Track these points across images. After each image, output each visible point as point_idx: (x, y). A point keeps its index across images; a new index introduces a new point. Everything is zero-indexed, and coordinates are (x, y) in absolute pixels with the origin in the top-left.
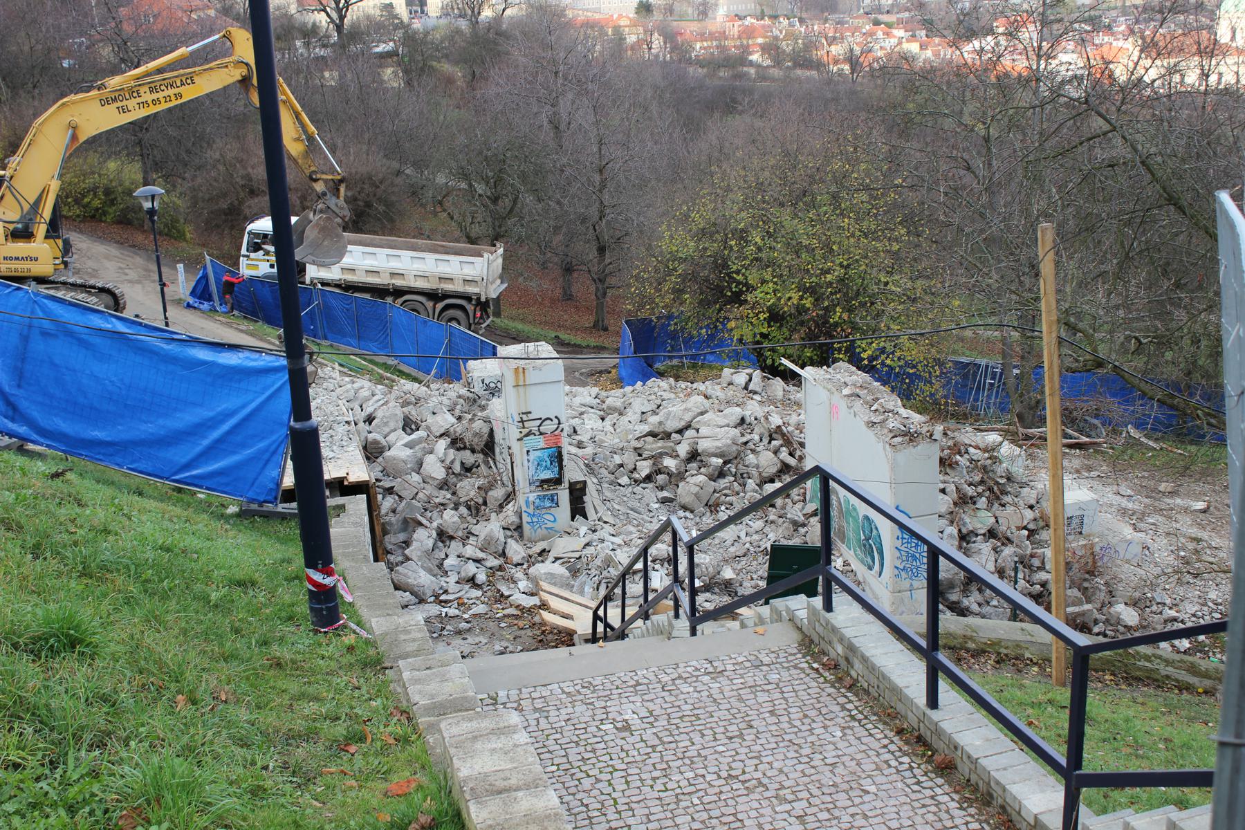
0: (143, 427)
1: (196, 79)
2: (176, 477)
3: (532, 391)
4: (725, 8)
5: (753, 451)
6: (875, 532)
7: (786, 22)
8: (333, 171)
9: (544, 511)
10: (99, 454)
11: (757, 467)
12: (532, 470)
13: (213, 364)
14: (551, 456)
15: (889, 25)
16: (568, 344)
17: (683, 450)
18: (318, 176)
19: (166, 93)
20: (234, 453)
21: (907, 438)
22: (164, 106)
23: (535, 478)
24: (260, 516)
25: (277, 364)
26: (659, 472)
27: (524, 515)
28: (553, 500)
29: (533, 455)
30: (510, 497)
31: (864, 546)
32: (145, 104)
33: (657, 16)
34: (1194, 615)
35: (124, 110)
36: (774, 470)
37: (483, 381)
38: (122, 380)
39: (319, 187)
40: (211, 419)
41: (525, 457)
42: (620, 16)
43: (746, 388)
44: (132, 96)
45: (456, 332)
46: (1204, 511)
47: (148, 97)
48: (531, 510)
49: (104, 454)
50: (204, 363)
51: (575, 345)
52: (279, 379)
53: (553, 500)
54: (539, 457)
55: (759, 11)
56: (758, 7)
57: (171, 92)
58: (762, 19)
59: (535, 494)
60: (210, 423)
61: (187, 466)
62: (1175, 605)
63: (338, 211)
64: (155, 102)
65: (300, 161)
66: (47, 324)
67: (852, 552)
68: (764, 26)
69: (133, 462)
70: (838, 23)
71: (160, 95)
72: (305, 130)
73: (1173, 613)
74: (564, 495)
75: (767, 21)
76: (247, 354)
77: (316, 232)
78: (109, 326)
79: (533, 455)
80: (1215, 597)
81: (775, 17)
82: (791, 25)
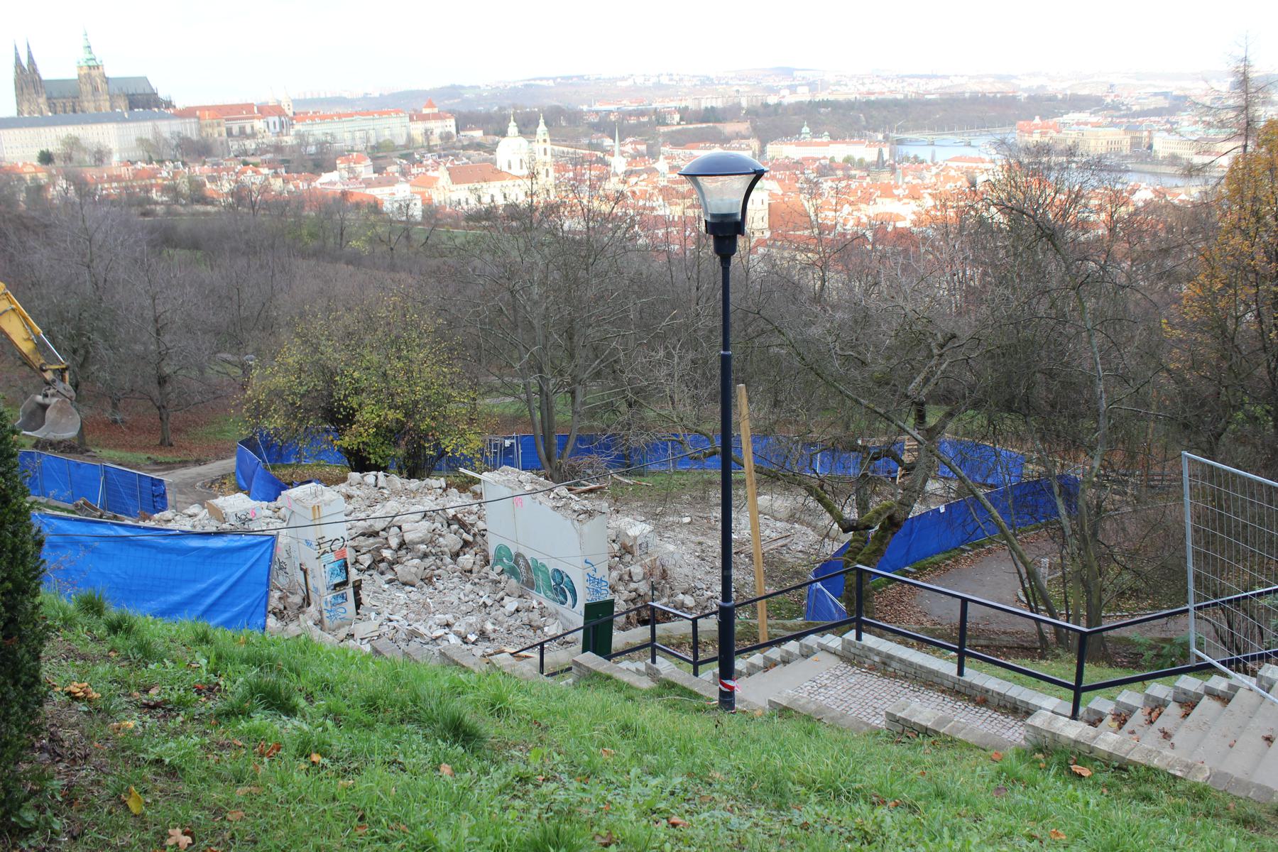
4: (118, 155)
5: (440, 535)
7: (171, 165)
11: (446, 546)
12: (328, 578)
14: (340, 566)
15: (256, 165)
16: (161, 463)
17: (394, 542)
20: (225, 612)
27: (325, 612)
29: (328, 567)
30: (307, 601)
31: (556, 589)
33: (59, 163)
40: (204, 590)
42: (25, 164)
45: (112, 471)
46: (689, 523)
48: (329, 608)
51: (168, 463)
52: (257, 552)
55: (147, 158)
56: (146, 154)
58: (151, 163)
63: (65, 393)
65: (31, 357)
67: (542, 595)
68: (153, 169)
70: (214, 165)
73: (709, 593)
74: (350, 591)
75: (155, 165)
76: (230, 537)
78: (112, 533)
79: (328, 567)
81: (161, 162)
82: (175, 167)
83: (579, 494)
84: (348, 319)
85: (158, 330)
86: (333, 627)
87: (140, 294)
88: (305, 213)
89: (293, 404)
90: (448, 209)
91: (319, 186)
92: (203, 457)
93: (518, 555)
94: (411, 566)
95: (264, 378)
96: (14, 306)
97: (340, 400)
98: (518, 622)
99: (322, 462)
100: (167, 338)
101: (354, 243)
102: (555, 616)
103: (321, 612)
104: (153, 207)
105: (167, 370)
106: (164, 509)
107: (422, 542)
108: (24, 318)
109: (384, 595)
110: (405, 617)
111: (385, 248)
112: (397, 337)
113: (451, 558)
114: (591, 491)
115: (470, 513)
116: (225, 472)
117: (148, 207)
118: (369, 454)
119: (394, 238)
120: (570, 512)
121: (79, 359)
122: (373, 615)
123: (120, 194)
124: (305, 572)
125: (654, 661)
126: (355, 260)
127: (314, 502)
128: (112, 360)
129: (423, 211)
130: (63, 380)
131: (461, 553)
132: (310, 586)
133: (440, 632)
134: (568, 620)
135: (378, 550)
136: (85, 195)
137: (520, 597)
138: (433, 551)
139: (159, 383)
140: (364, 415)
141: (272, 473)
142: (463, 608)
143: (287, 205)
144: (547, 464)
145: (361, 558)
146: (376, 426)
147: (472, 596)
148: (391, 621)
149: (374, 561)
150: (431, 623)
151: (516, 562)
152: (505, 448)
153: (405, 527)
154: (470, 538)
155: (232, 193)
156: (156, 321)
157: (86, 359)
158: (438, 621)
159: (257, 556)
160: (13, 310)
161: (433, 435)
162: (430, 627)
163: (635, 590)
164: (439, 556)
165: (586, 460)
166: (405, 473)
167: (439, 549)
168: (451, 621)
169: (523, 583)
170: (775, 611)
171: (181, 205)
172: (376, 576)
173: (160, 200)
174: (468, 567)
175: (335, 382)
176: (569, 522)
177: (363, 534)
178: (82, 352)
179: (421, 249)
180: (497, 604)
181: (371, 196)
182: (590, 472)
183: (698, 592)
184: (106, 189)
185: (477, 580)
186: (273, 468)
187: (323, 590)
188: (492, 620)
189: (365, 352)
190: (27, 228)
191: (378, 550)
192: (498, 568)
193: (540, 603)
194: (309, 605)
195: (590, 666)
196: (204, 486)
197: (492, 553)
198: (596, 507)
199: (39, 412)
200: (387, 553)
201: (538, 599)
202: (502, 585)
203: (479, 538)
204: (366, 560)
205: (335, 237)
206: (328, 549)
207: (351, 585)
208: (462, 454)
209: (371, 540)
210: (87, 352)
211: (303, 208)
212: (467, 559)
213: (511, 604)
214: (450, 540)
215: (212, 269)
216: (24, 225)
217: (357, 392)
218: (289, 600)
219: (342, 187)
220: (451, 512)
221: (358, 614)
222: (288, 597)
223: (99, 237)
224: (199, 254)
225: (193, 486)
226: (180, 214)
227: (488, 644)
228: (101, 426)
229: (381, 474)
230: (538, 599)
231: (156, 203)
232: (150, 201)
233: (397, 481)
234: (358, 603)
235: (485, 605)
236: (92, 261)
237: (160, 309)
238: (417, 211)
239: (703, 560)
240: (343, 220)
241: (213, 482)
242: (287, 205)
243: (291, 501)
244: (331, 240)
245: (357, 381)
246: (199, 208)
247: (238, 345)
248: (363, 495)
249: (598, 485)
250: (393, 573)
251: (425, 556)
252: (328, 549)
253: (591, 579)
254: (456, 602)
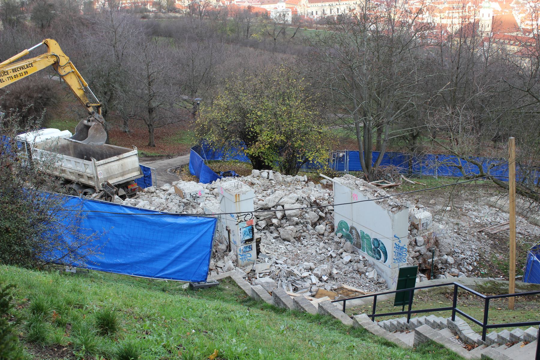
0: (140, 255)
1: (33, 64)
2: (158, 275)
3: (241, 203)
5: (306, 212)
6: (381, 245)
8: (96, 102)
9: (247, 253)
10: (119, 269)
11: (309, 219)
12: (242, 236)
13: (176, 224)
14: (249, 230)
17: (279, 215)
18: (90, 105)
19: (20, 72)
20: (185, 262)
21: (398, 208)
22: (20, 78)
23: (243, 240)
24: (201, 288)
25: (205, 221)
27: (239, 256)
28: (250, 248)
29: (243, 230)
32: (11, 78)
34: (470, 256)
36: (316, 220)
37: (190, 194)
38: (129, 235)
39: (91, 110)
40: (173, 248)
41: (239, 231)
43: (268, 178)
44: (4, 75)
46: (450, 211)
47: (13, 74)
48: (241, 254)
49: (121, 269)
50: (170, 224)
51: (152, 156)
53: (250, 248)
54: (245, 231)
57: (22, 71)
59: (243, 246)
60: (173, 250)
61: (163, 270)
62: (462, 252)
63: (100, 120)
64: (16, 76)
65: (81, 99)
66: (89, 213)
67: (366, 253)
69: (136, 271)
71: (18, 73)
73: (463, 256)
74: (254, 244)
76: (191, 218)
77: (93, 130)
78: (122, 212)
80: (474, 247)
83: (384, 188)
84: (256, 81)
85: (149, 82)
86: (243, 264)
87: (141, 63)
88: (228, 18)
89: (223, 128)
90: (306, 17)
91: (236, 3)
92: (171, 154)
93: (352, 228)
94: (289, 230)
95: (207, 112)
96: (73, 70)
97: (249, 127)
98: (351, 269)
99: (236, 161)
100: (154, 88)
101: (254, 35)
102: (373, 266)
103: (237, 256)
104: (148, 13)
105: (154, 105)
106: (150, 185)
107: (295, 216)
108: (79, 77)
109: (272, 246)
110: (285, 262)
111: (271, 38)
112: (283, 93)
113: (312, 226)
114: (390, 187)
115: (324, 199)
116: (183, 163)
117: (145, 13)
118: (264, 159)
119: (276, 33)
120: (387, 206)
121: (108, 98)
122: (267, 259)
123: (131, 6)
124: (229, 232)
125: (453, 319)
126: (255, 45)
127: (237, 191)
128: (125, 99)
129: (292, 18)
130: (98, 112)
131: (318, 224)
132: (231, 240)
133: (306, 274)
134: (380, 269)
135: (270, 219)
136: (113, 7)
137: (352, 253)
138: (302, 221)
139: (149, 112)
140: (263, 137)
141: (208, 165)
142: (319, 257)
143: (219, 13)
144: (366, 170)
145: (259, 223)
146: (269, 144)
147: (324, 250)
148: (277, 264)
149: (267, 225)
150: (301, 268)
151: (351, 232)
152: (340, 158)
153: (286, 207)
154: (323, 215)
155: (189, 7)
156: (149, 77)
157: (111, 97)
158: (305, 267)
159: (206, 229)
160: (73, 72)
161: (302, 151)
162: (301, 270)
163: (419, 251)
164: (305, 224)
165: (388, 168)
166: (284, 172)
167: (305, 220)
168: (313, 266)
169: (354, 244)
170: (503, 270)
171: (163, 13)
172: (268, 234)
173: (151, 10)
174: (322, 232)
175: (247, 118)
176: (386, 211)
177: (261, 209)
178: (109, 93)
179: (291, 39)
180: (338, 256)
181: (264, 9)
182: (389, 175)
183: (456, 255)
184: (124, 3)
185: (327, 241)
186: (209, 162)
187: (239, 243)
188: (335, 266)
189: (265, 100)
190: (83, 24)
191: (270, 219)
192: (339, 235)
193: (364, 258)
194: (230, 251)
195: (427, 335)
196: (171, 171)
197: (336, 225)
198: (403, 204)
199: (85, 130)
200: (275, 221)
201: (364, 254)
202: (342, 245)
203: (328, 215)
204: (263, 224)
205: (244, 32)
206: (243, 220)
207: (255, 241)
208: (317, 162)
209: (266, 213)
210: (112, 94)
211: (227, 15)
212: (321, 228)
213: (347, 257)
214: (312, 215)
215: (179, 48)
216: (83, 23)
217: (259, 123)
218: (219, 247)
219: (248, 4)
220: (313, 199)
221: (258, 258)
222: (218, 245)
223: (120, 30)
224: (171, 40)
225: (166, 171)
226: (162, 18)
227: (334, 282)
228: (118, 134)
229: (271, 171)
230: (364, 254)
231: (150, 12)
232: (147, 10)
233: (280, 176)
234: (258, 252)
235: (331, 256)
236: (116, 43)
237: (151, 71)
238: (289, 18)
239: (459, 234)
240: (249, 22)
241: (176, 169)
242: (219, 13)
243: (223, 190)
244: (242, 33)
245: (260, 116)
246: (172, 14)
247: (193, 92)
248: (260, 183)
249: (394, 184)
250: (277, 233)
251: (297, 224)
252: (243, 220)
253: (397, 247)
254: (314, 253)
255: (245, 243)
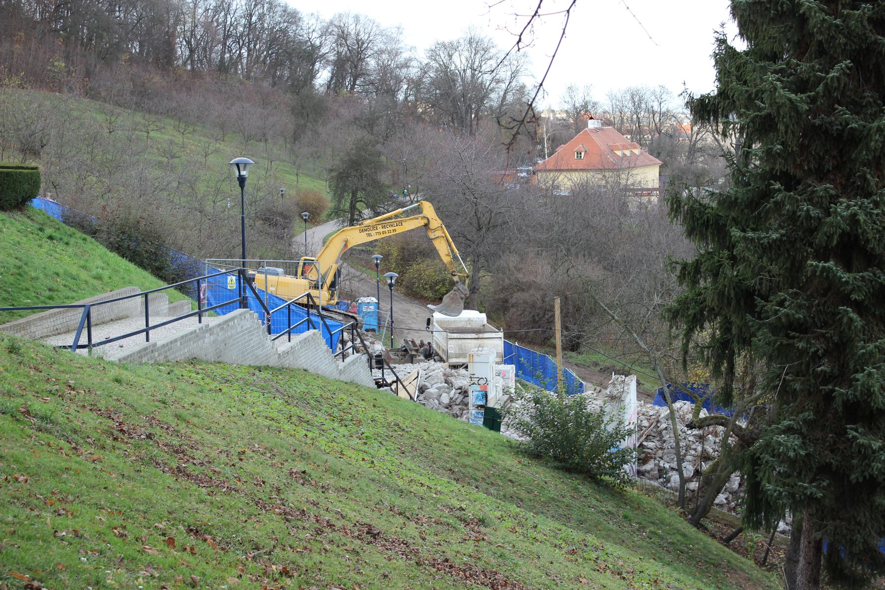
1: (403, 223)
14: (482, 395)
19: (389, 229)
22: (388, 235)
26: (380, 362)
29: (475, 393)
35: (369, 235)
47: (380, 230)
48: (473, 418)
57: (391, 228)
71: (386, 230)
72: (452, 251)
130: (464, 283)
206: (476, 382)
252: (476, 382)
255: (477, 408)
